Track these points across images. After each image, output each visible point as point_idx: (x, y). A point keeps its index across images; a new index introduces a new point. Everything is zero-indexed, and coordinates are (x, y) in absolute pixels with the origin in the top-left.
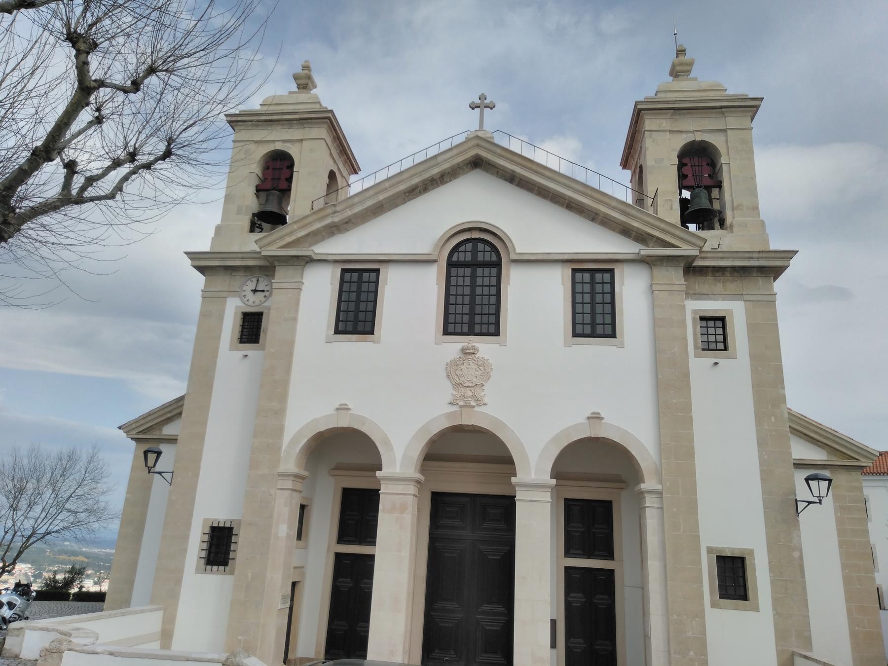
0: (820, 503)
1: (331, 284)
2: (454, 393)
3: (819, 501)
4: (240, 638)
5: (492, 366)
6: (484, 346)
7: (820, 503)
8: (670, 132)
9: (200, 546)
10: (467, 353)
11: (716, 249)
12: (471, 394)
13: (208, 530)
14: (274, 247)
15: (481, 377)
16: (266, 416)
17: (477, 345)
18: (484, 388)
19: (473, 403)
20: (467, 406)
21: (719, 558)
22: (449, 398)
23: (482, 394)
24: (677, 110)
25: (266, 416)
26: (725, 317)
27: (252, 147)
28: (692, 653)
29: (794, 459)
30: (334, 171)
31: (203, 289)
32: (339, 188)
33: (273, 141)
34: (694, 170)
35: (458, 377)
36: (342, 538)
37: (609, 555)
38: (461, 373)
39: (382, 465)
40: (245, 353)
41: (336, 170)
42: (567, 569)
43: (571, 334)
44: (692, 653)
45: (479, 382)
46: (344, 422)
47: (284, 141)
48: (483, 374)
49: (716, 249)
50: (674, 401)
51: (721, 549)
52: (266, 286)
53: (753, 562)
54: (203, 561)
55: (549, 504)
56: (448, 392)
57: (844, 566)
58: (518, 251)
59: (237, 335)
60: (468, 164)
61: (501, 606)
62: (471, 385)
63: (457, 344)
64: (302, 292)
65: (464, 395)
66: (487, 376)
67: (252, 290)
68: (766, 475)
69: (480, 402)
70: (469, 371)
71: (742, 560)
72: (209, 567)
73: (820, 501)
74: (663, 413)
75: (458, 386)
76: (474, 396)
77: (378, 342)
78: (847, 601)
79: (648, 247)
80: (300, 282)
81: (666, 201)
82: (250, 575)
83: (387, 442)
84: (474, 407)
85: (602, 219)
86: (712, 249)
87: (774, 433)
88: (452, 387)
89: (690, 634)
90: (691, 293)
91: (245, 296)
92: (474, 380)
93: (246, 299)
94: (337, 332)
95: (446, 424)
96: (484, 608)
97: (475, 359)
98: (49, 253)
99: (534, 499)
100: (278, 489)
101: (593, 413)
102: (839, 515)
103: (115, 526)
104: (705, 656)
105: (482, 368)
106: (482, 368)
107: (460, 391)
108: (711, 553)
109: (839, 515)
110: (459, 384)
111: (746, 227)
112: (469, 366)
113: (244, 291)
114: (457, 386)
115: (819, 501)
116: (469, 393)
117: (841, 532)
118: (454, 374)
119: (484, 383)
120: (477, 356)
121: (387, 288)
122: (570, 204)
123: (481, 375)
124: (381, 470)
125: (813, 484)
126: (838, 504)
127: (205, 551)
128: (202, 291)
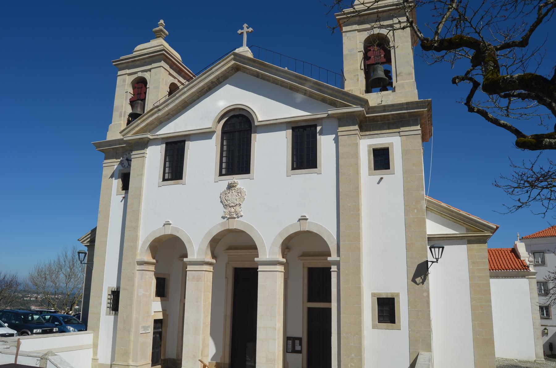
0: (437, 262)
1: (161, 152)
2: (225, 210)
3: (436, 261)
4: (122, 348)
5: (245, 192)
6: (240, 180)
7: (437, 262)
10: (230, 187)
11: (380, 104)
12: (234, 210)
13: (110, 293)
14: (129, 135)
15: (239, 199)
16: (130, 231)
17: (236, 181)
18: (241, 206)
19: (235, 216)
21: (378, 299)
23: (240, 210)
24: (361, 16)
25: (130, 231)
26: (388, 147)
27: (127, 76)
28: (353, 355)
29: (428, 235)
30: (175, 82)
35: (227, 201)
38: (228, 198)
39: (187, 254)
41: (176, 82)
43: (291, 168)
44: (353, 355)
45: (238, 203)
46: (168, 231)
47: (142, 71)
48: (240, 198)
49: (380, 104)
50: (349, 205)
51: (379, 294)
53: (399, 300)
56: (221, 210)
57: (472, 299)
58: (259, 120)
60: (232, 69)
62: (233, 205)
65: (230, 211)
68: (409, 246)
70: (232, 197)
71: (393, 299)
73: (437, 260)
74: (342, 213)
78: (473, 320)
79: (338, 108)
80: (144, 153)
81: (355, 76)
82: (125, 316)
83: (190, 242)
84: (235, 218)
85: (310, 94)
86: (378, 104)
87: (416, 220)
89: (352, 344)
91: (123, 163)
92: (235, 202)
93: (124, 165)
95: (220, 229)
97: (236, 189)
98: (468, 34)
100: (137, 270)
101: (302, 216)
102: (471, 267)
104: (360, 356)
105: (240, 194)
106: (240, 194)
107: (228, 209)
109: (471, 267)
111: (403, 87)
112: (232, 194)
114: (225, 206)
115: (436, 261)
116: (233, 210)
117: (471, 278)
119: (241, 203)
120: (237, 187)
123: (239, 199)
124: (187, 257)
125: (433, 249)
126: (471, 261)
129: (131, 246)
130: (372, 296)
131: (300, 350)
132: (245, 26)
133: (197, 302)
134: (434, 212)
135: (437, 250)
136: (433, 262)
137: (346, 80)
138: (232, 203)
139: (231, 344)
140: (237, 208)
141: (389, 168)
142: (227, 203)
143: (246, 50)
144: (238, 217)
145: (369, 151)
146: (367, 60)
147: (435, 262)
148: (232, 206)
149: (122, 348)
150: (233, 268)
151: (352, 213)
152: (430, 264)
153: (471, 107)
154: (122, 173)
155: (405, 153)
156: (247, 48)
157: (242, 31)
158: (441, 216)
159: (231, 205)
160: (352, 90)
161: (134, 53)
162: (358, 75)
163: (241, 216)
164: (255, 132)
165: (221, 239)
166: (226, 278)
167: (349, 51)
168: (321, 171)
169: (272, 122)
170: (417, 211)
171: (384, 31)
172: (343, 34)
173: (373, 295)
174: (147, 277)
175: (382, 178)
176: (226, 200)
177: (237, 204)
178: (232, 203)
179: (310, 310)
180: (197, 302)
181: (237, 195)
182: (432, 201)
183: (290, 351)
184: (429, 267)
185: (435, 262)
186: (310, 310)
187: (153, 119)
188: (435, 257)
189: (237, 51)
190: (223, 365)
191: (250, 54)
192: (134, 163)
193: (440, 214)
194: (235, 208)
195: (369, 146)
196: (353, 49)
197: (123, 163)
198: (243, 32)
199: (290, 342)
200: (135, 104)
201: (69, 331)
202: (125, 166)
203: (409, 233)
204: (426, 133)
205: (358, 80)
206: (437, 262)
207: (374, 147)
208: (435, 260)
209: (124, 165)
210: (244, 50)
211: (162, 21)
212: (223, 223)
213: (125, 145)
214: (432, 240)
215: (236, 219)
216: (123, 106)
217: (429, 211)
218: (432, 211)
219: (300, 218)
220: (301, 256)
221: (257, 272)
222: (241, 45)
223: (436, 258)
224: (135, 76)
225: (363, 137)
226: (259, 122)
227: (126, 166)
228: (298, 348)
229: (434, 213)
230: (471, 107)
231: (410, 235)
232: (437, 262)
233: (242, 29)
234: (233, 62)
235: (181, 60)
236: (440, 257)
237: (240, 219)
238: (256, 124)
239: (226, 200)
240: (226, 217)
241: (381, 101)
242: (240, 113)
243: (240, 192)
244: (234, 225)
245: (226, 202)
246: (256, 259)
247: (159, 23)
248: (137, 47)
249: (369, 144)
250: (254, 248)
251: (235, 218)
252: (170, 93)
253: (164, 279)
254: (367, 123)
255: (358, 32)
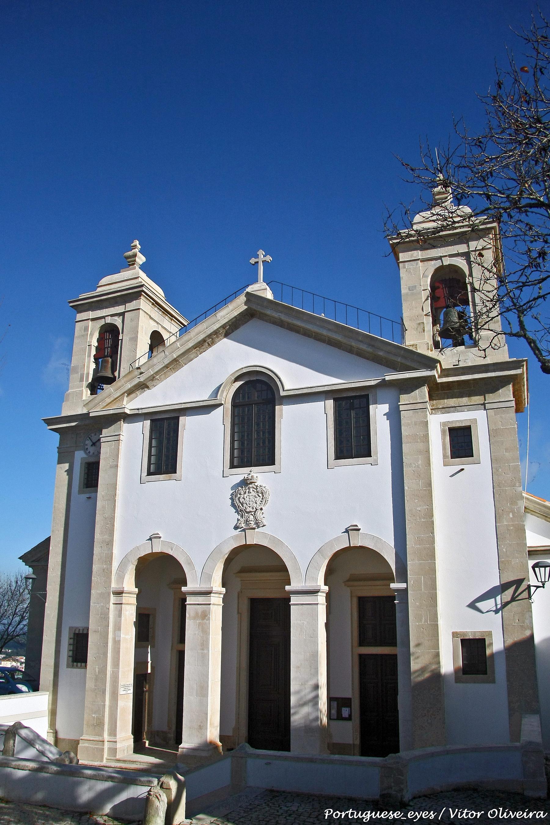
0: (543, 587)
3: (542, 586)
4: (94, 715)
7: (543, 587)
8: (423, 261)
9: (68, 648)
11: (457, 365)
13: (72, 636)
29: (528, 547)
31: (58, 446)
33: (104, 317)
40: (88, 495)
42: (361, 656)
47: (112, 315)
49: (457, 365)
50: (419, 509)
51: (464, 634)
54: (71, 659)
56: (233, 517)
59: (454, 425)
63: (242, 473)
66: (264, 500)
67: (92, 445)
72: (75, 664)
73: (544, 584)
81: (419, 324)
83: (190, 563)
84: (254, 529)
86: (454, 365)
87: (512, 528)
90: (441, 407)
91: (87, 448)
93: (88, 452)
94: (149, 474)
106: (260, 495)
108: (456, 637)
113: (86, 445)
115: (542, 586)
120: (256, 484)
122: (330, 340)
124: (289, 584)
125: (537, 569)
127: (71, 651)
128: (58, 448)
129: (104, 570)
130: (453, 637)
131: (332, 702)
132: (261, 253)
133: (203, 650)
134: (535, 514)
135: (542, 569)
136: (538, 587)
137: (407, 330)
138: (250, 507)
141: (472, 456)
142: (242, 508)
143: (263, 287)
144: (258, 527)
145: (443, 432)
146: (436, 302)
147: (541, 587)
149: (94, 715)
150: (248, 598)
151: (423, 520)
152: (533, 589)
154: (86, 463)
155: (492, 434)
156: (265, 285)
157: (256, 260)
158: (546, 520)
159: (248, 510)
160: (417, 345)
161: (99, 289)
162: (423, 323)
164: (281, 404)
165: (233, 559)
166: (238, 613)
167: (409, 289)
168: (376, 461)
170: (513, 515)
171: (461, 263)
172: (401, 265)
173: (455, 635)
174: (127, 613)
175: (463, 469)
176: (240, 502)
178: (250, 507)
179: (362, 658)
180: (203, 650)
182: (532, 499)
183: (335, 717)
184: (532, 594)
185: (541, 587)
186: (362, 658)
187: (132, 387)
188: (540, 580)
189: (249, 289)
190: (237, 740)
191: (269, 295)
192: (105, 449)
193: (544, 517)
195: (444, 424)
196: (416, 286)
197: (87, 448)
198: (258, 262)
199: (335, 704)
201: (20, 691)
202: (89, 452)
203: (503, 546)
204: (520, 401)
205: (424, 331)
206: (544, 588)
207: (451, 426)
208: (541, 584)
209: (88, 452)
210: (261, 288)
211: (137, 242)
212: (235, 538)
214: (534, 554)
215: (256, 530)
216: (84, 365)
217: (528, 513)
218: (533, 513)
220: (348, 581)
221: (289, 606)
222: (256, 281)
223: (541, 582)
224: (102, 322)
225: (434, 412)
226: (285, 391)
227: (91, 454)
228: (345, 712)
229: (535, 515)
231: (504, 550)
232: (544, 588)
233: (257, 256)
235: (164, 297)
236: (547, 580)
238: (282, 393)
239: (240, 502)
241: (459, 361)
243: (261, 493)
244: (254, 538)
246: (287, 588)
247: (132, 245)
248: (103, 279)
249: (442, 421)
250: (283, 569)
251: (254, 529)
252: (152, 348)
253: (148, 616)
254: (439, 391)
255: (421, 261)
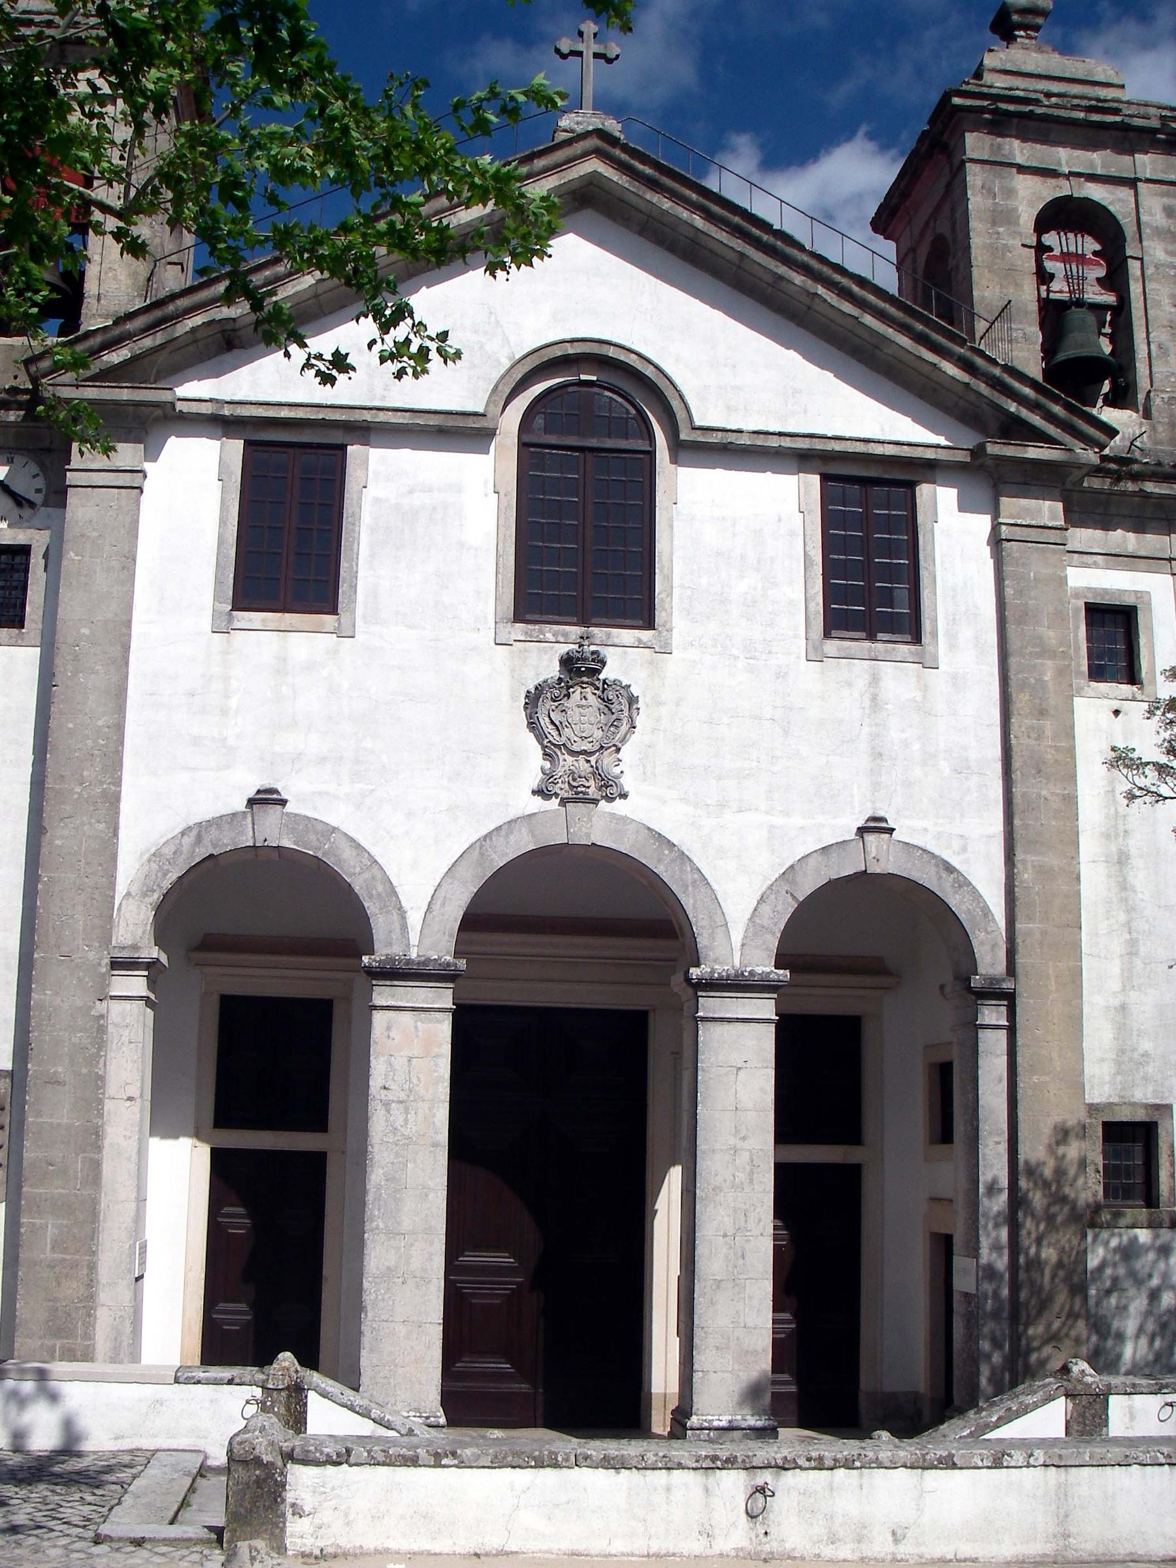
19: (593, 792)
20: (579, 798)
22: (534, 778)
23: (617, 770)
32: (192, 249)
34: (1068, 269)
36: (851, 1175)
37: (852, 1134)
52: (34, 477)
55: (772, 1028)
58: (698, 422)
61: (507, 1254)
64: (144, 498)
65: (573, 773)
69: (610, 789)
75: (557, 750)
76: (597, 773)
77: (345, 633)
88: (541, 752)
96: (466, 1259)
99: (716, 1016)
103: (986, 1330)
110: (558, 746)
118: (547, 719)
120: (602, 677)
121: (368, 495)
139: (646, 1343)
140: (607, 759)
144: (610, 799)
148: (584, 752)
153: (229, 36)
159: (575, 748)
163: (624, 796)
169: (284, 413)
176: (552, 723)
177: (602, 747)
181: (606, 710)
194: (593, 759)
200: (73, 513)
213: (833, 606)
219: (861, 823)
230: (229, 36)
234: (593, 165)
237: (619, 806)
239: (552, 723)
240: (556, 795)
242: (1127, 159)
245: (555, 733)
251: (595, 802)
